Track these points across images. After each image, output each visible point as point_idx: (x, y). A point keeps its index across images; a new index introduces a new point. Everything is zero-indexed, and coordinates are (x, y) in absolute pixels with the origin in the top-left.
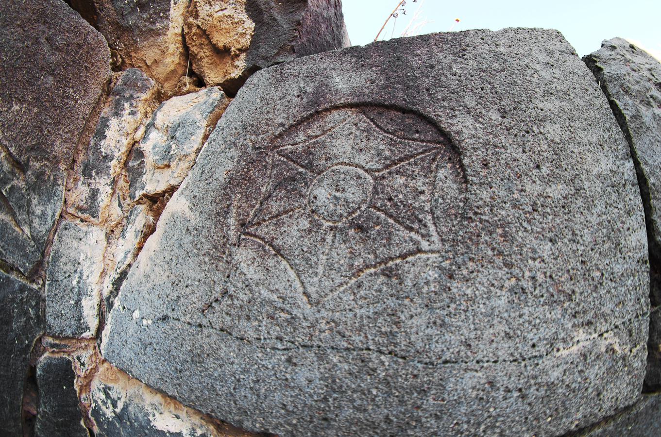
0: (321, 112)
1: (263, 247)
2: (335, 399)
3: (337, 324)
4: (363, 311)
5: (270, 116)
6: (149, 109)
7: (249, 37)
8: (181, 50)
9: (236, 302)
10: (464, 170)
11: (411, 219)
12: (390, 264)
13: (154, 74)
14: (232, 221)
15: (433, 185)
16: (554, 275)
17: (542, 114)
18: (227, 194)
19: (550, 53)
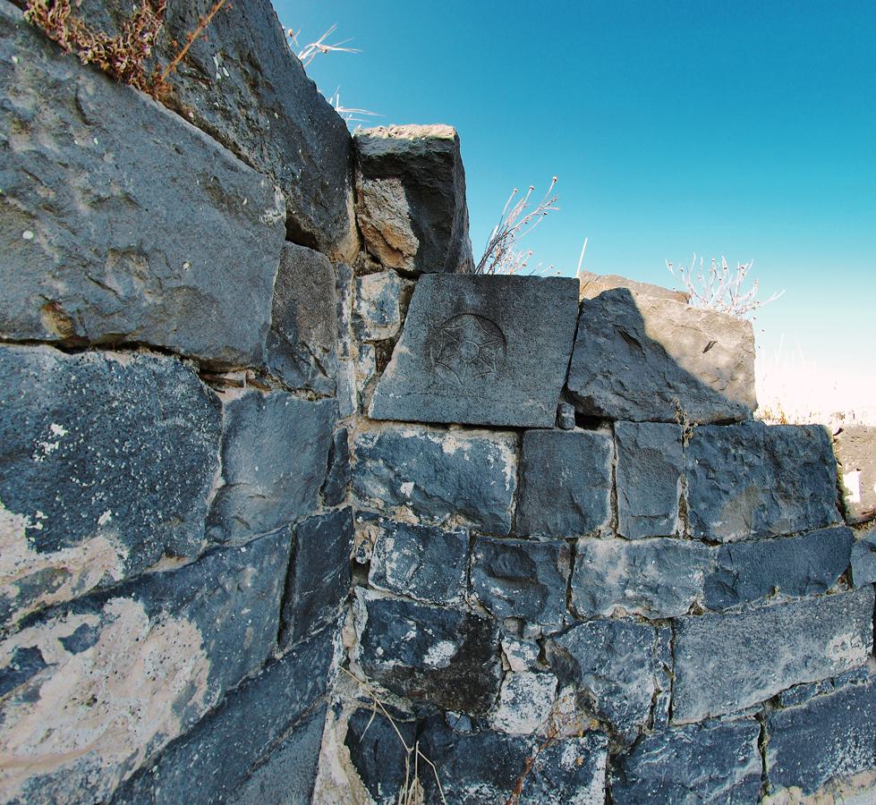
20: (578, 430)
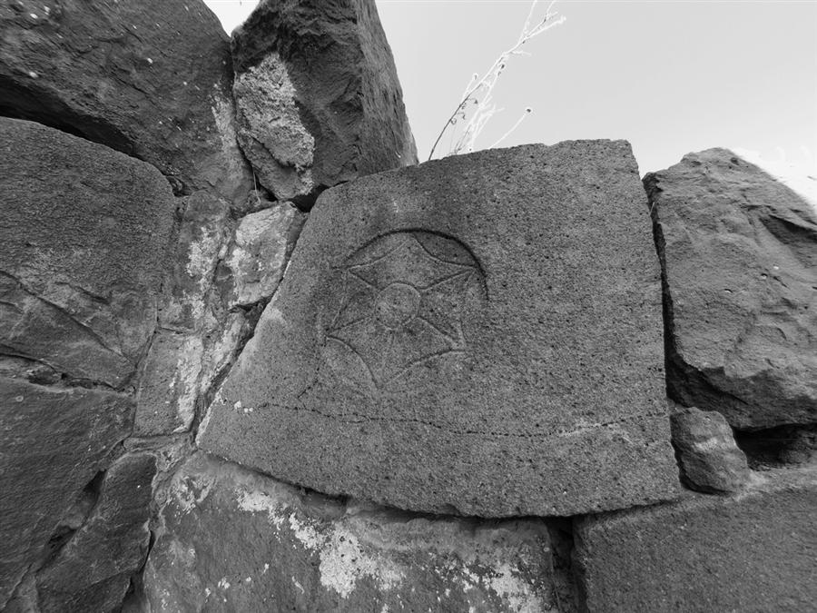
0: (382, 236)
1: (343, 347)
2: (394, 460)
3: (395, 402)
4: (412, 392)
5: (342, 238)
6: (226, 229)
7: (311, 153)
8: (242, 164)
9: (324, 388)
10: (487, 290)
11: (446, 327)
12: (431, 358)
13: (221, 192)
14: (318, 327)
15: (463, 299)
16: (553, 373)
17: (566, 240)
18: (313, 306)
19: (602, 172)
20: (758, 480)
